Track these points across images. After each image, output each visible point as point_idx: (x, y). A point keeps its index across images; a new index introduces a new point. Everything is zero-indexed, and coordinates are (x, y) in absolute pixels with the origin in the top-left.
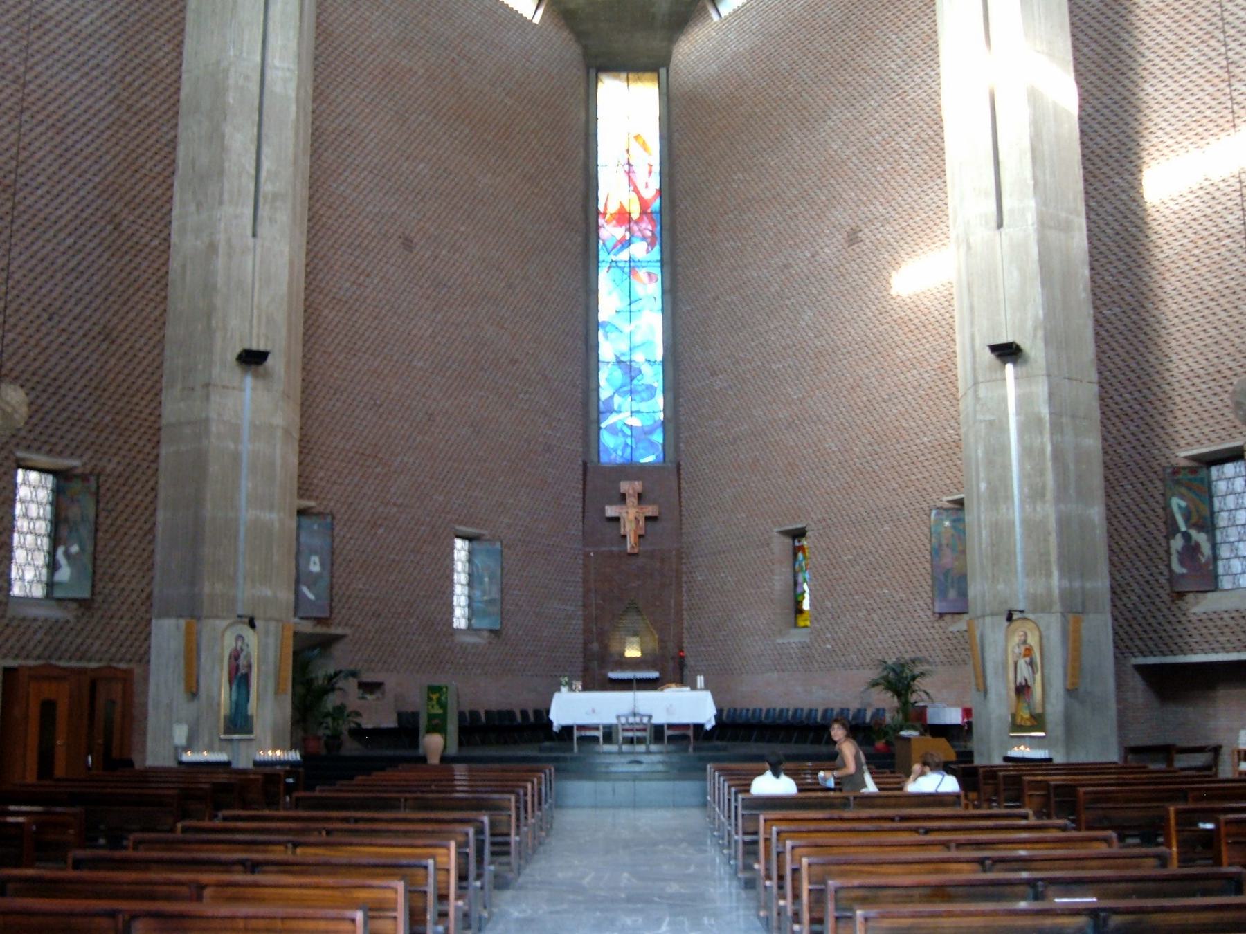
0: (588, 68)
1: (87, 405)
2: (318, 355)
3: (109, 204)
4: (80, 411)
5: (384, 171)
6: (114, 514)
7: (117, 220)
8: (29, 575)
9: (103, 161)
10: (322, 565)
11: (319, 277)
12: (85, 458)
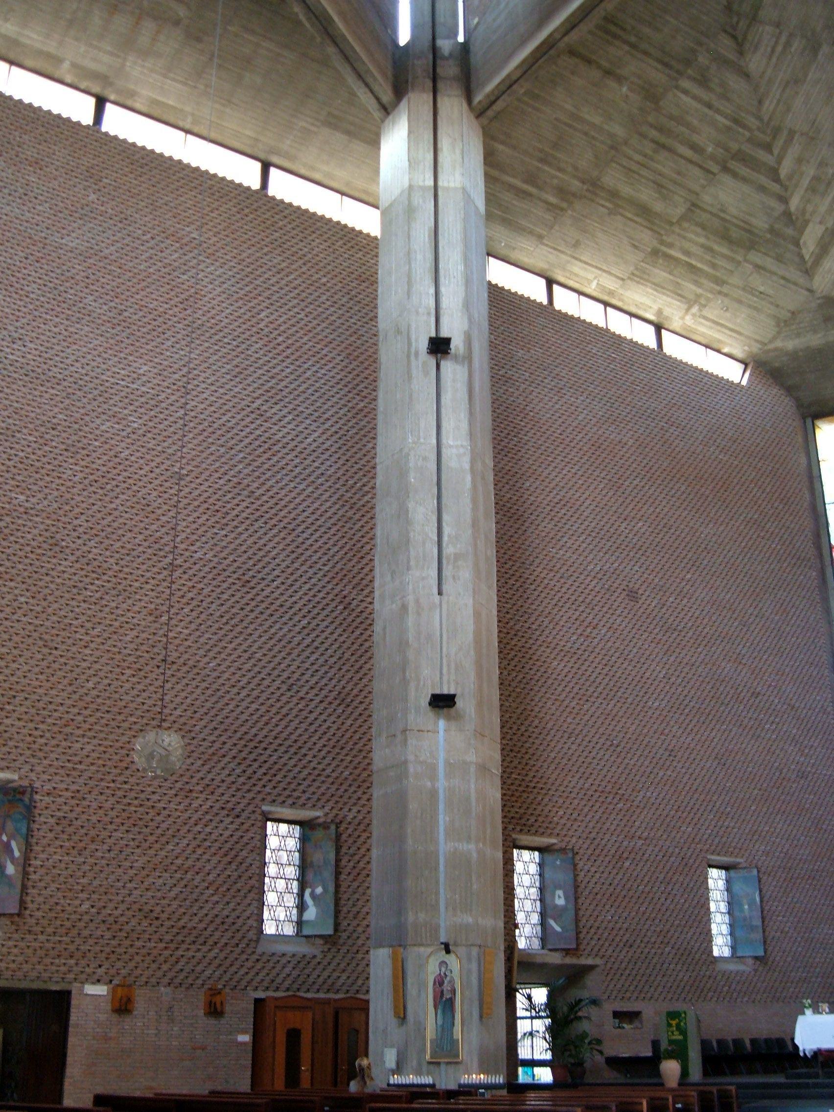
0: (804, 418)
1: (326, 761)
2: (549, 703)
3: (339, 588)
4: (321, 767)
5: (603, 532)
6: (357, 858)
7: (347, 600)
8: (281, 914)
9: (331, 552)
10: (566, 898)
11: (547, 632)
12: (327, 809)
